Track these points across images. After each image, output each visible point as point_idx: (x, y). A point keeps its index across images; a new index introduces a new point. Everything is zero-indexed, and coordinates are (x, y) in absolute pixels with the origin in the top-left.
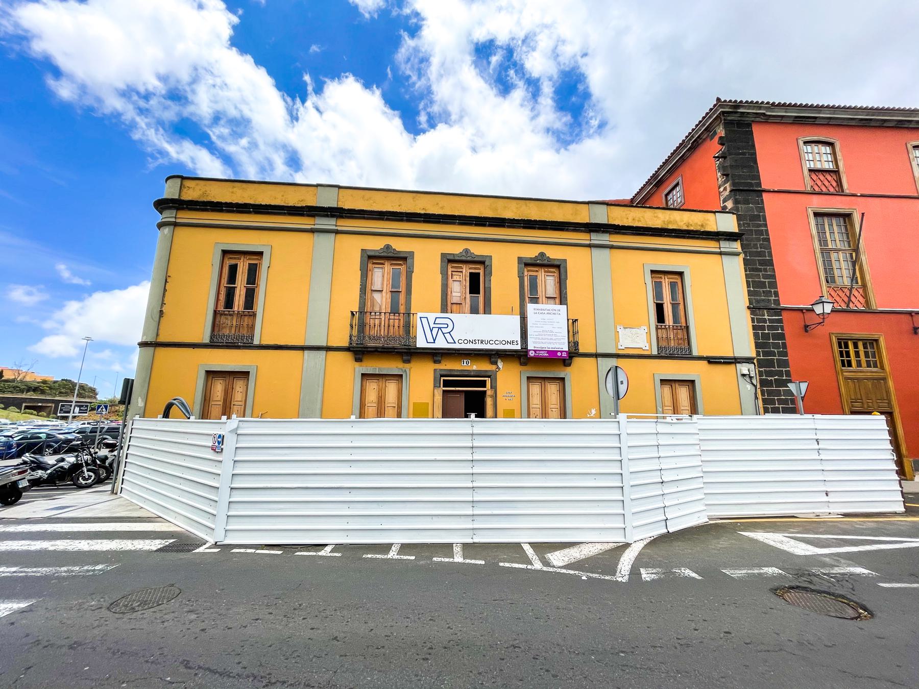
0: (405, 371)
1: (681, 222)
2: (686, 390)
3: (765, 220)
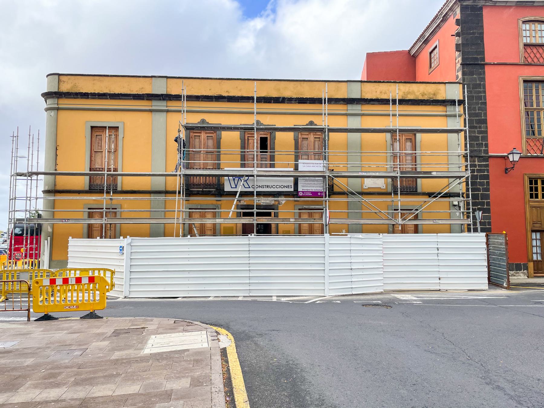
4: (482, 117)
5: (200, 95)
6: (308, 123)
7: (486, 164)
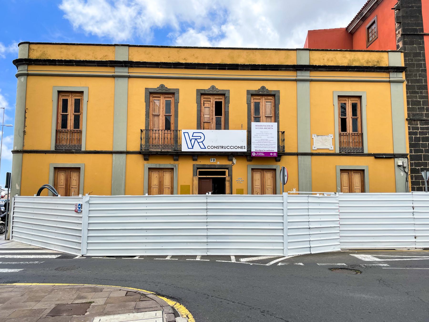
0: (175, 166)
1: (363, 60)
2: (358, 176)
3: (424, 56)
4: (423, 83)
5: (159, 62)
6: (260, 88)
7: (427, 127)
